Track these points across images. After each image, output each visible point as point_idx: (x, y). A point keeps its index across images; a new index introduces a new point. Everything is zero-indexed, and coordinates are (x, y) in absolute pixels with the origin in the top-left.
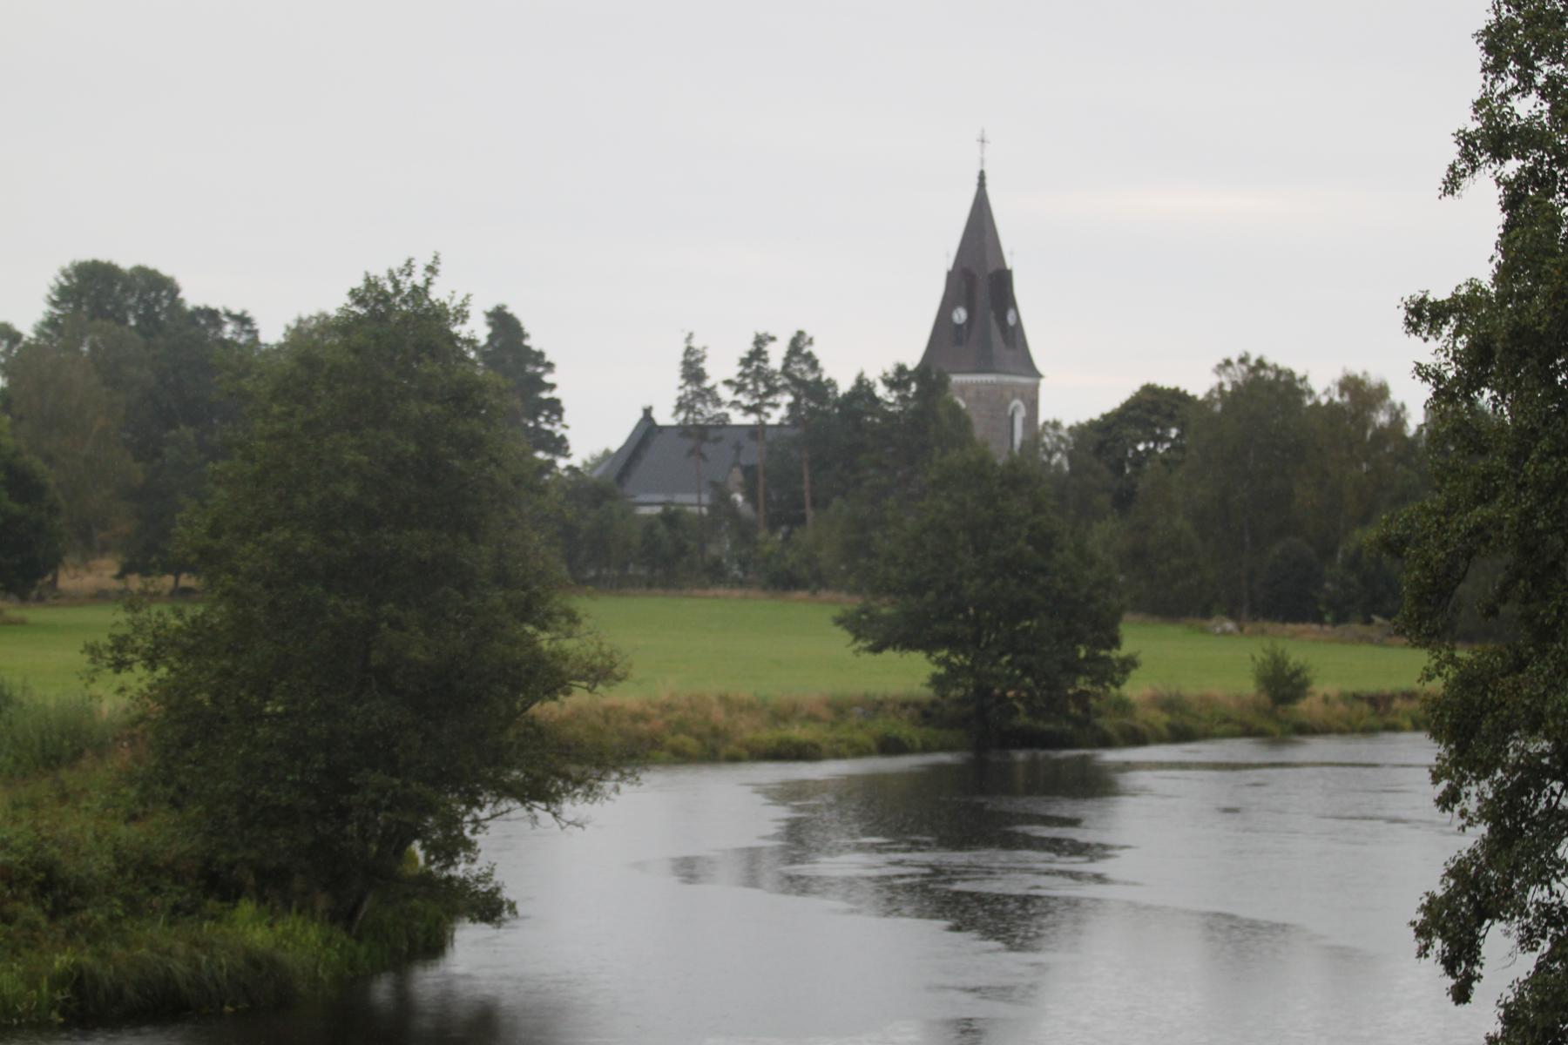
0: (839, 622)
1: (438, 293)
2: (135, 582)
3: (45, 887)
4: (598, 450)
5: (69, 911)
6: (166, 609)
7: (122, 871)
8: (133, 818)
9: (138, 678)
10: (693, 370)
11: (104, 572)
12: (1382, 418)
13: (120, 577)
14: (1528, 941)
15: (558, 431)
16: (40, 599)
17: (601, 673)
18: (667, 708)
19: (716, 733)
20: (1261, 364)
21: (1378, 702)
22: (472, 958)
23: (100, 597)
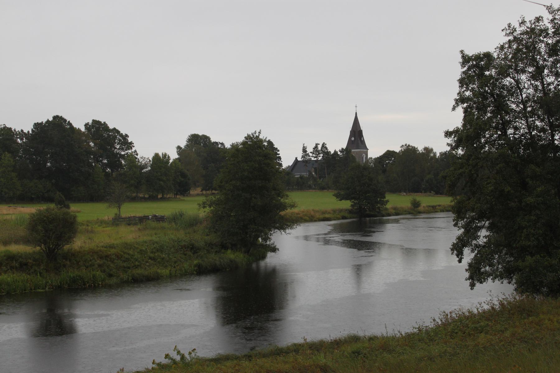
0: (334, 195)
1: (261, 137)
2: (204, 192)
3: (192, 249)
4: (287, 166)
5: (197, 253)
6: (213, 197)
7: (206, 245)
8: (208, 235)
9: (208, 209)
10: (304, 150)
11: (199, 190)
12: (432, 155)
13: (201, 191)
14: (473, 251)
15: (280, 162)
16: (187, 196)
17: (293, 206)
18: (303, 212)
19: (312, 216)
20: (409, 145)
21: (434, 207)
22: (271, 260)
23: (198, 195)
